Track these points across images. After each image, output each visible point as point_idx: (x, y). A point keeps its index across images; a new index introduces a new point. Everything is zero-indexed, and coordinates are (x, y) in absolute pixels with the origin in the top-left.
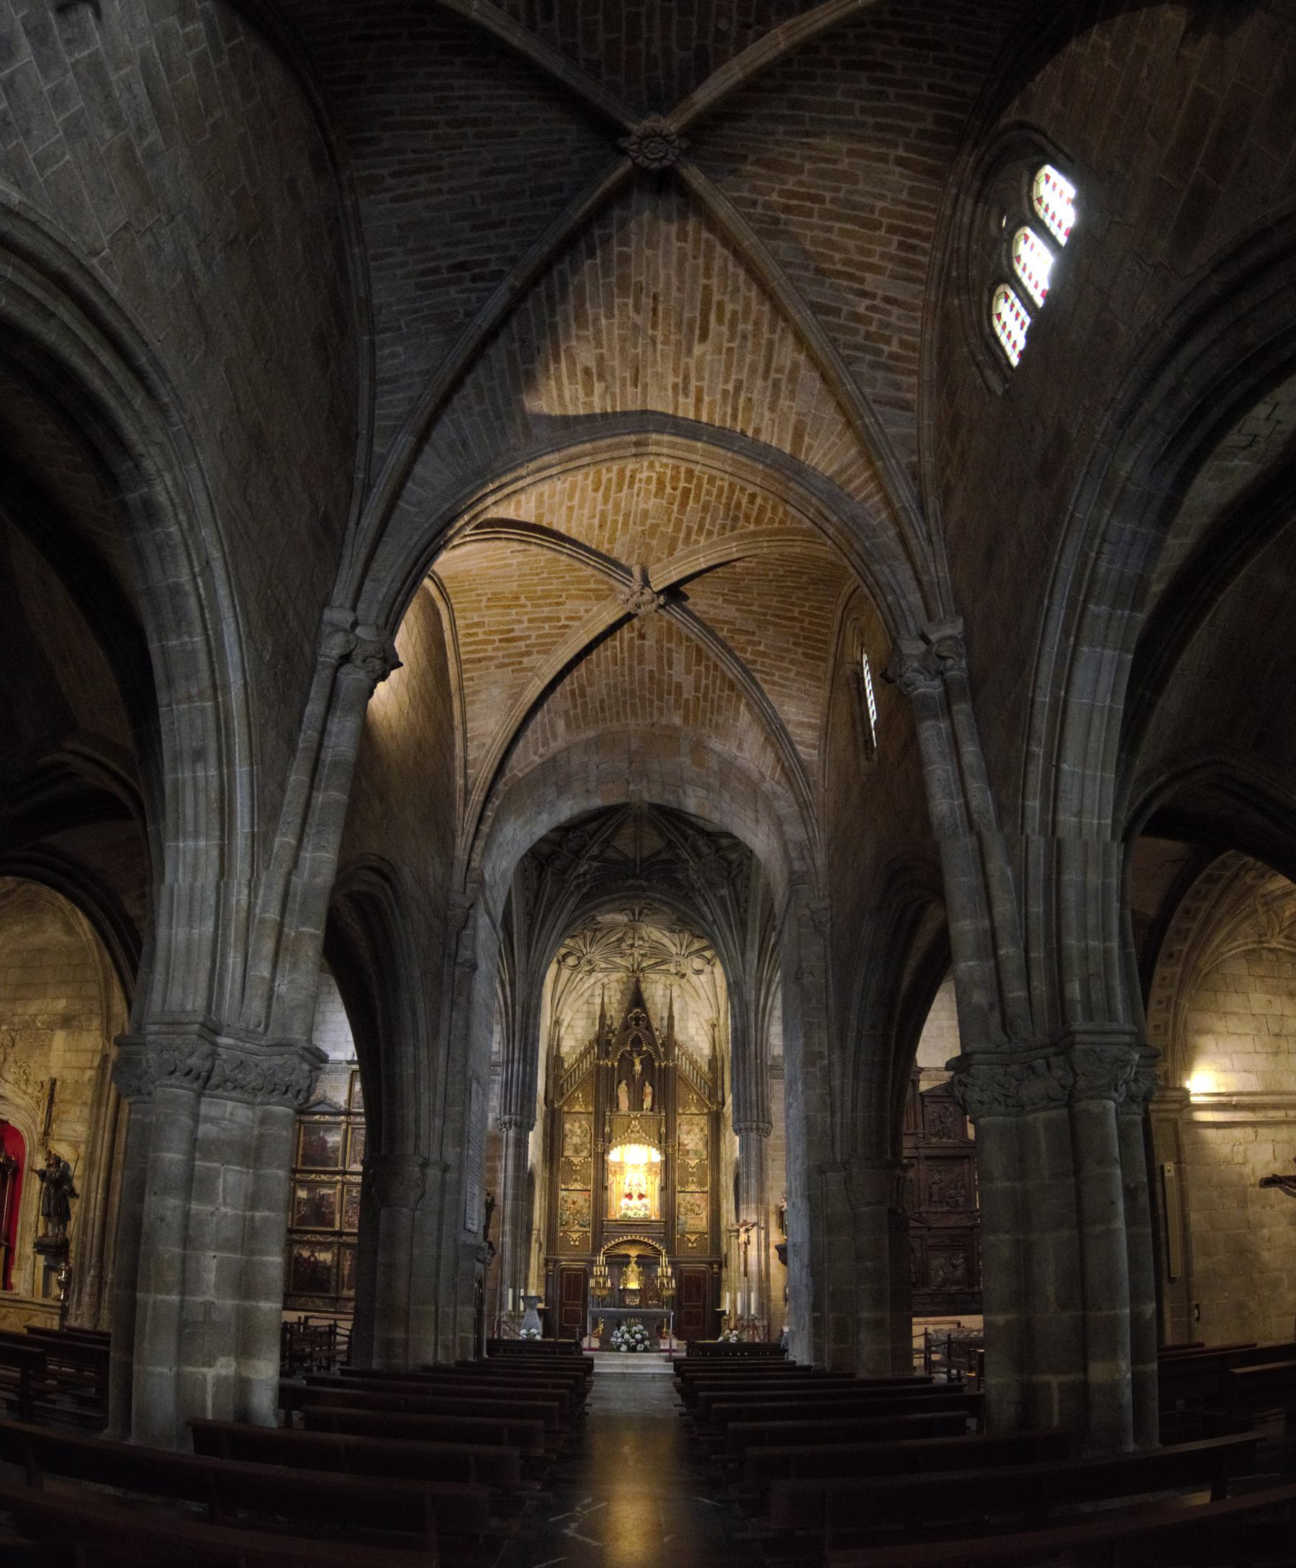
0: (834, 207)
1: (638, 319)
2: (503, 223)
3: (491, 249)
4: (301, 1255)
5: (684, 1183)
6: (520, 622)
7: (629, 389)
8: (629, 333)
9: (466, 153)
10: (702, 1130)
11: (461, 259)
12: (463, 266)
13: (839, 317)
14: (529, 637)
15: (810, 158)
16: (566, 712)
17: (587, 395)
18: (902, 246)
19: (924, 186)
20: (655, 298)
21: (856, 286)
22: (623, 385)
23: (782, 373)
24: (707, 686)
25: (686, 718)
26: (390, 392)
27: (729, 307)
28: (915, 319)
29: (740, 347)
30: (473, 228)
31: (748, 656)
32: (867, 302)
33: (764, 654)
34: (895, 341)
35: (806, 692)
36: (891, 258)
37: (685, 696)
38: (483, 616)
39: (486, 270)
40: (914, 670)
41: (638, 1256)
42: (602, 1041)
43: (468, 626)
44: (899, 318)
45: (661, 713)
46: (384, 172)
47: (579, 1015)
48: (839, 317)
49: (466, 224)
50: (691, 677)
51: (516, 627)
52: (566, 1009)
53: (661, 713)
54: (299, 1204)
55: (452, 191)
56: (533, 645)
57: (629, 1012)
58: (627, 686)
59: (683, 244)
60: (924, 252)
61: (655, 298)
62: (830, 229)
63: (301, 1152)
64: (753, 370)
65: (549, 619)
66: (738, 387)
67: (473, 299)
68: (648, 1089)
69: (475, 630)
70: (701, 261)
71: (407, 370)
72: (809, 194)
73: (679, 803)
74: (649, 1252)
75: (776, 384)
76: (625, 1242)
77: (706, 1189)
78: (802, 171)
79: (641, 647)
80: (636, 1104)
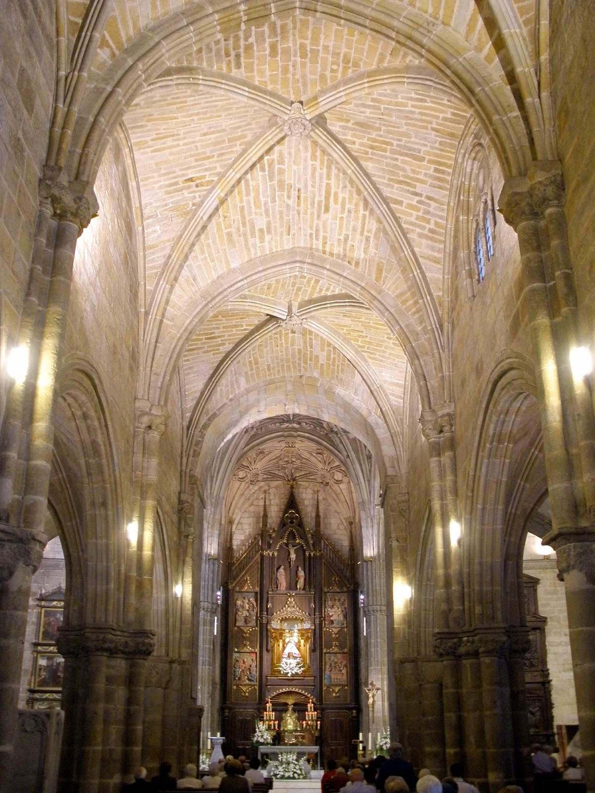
0: (398, 149)
1: (290, 202)
3: (206, 170)
6: (218, 328)
7: (285, 237)
8: (284, 210)
10: (342, 604)
11: (189, 177)
12: (191, 180)
13: (402, 206)
15: (384, 125)
16: (246, 373)
17: (261, 242)
18: (436, 170)
19: (449, 141)
20: (299, 190)
21: (411, 189)
22: (282, 235)
23: (371, 233)
24: (334, 358)
27: (341, 196)
28: (443, 210)
29: (347, 217)
30: (196, 160)
32: (418, 198)
33: (370, 343)
34: (432, 221)
35: (396, 365)
36: (431, 176)
37: (321, 362)
39: (203, 180)
41: (295, 704)
44: (434, 209)
45: (306, 370)
47: (246, 515)
48: (402, 206)
50: (325, 353)
52: (237, 511)
53: (306, 370)
54: (40, 669)
57: (286, 512)
58: (285, 357)
59: (314, 162)
60: (449, 174)
61: (299, 190)
62: (396, 159)
63: (42, 630)
64: (354, 230)
65: (236, 326)
66: (346, 239)
67: (197, 197)
68: (301, 573)
70: (325, 170)
72: (385, 141)
74: (301, 699)
75: (368, 239)
77: (346, 650)
78: (380, 130)
79: (293, 338)
80: (292, 586)
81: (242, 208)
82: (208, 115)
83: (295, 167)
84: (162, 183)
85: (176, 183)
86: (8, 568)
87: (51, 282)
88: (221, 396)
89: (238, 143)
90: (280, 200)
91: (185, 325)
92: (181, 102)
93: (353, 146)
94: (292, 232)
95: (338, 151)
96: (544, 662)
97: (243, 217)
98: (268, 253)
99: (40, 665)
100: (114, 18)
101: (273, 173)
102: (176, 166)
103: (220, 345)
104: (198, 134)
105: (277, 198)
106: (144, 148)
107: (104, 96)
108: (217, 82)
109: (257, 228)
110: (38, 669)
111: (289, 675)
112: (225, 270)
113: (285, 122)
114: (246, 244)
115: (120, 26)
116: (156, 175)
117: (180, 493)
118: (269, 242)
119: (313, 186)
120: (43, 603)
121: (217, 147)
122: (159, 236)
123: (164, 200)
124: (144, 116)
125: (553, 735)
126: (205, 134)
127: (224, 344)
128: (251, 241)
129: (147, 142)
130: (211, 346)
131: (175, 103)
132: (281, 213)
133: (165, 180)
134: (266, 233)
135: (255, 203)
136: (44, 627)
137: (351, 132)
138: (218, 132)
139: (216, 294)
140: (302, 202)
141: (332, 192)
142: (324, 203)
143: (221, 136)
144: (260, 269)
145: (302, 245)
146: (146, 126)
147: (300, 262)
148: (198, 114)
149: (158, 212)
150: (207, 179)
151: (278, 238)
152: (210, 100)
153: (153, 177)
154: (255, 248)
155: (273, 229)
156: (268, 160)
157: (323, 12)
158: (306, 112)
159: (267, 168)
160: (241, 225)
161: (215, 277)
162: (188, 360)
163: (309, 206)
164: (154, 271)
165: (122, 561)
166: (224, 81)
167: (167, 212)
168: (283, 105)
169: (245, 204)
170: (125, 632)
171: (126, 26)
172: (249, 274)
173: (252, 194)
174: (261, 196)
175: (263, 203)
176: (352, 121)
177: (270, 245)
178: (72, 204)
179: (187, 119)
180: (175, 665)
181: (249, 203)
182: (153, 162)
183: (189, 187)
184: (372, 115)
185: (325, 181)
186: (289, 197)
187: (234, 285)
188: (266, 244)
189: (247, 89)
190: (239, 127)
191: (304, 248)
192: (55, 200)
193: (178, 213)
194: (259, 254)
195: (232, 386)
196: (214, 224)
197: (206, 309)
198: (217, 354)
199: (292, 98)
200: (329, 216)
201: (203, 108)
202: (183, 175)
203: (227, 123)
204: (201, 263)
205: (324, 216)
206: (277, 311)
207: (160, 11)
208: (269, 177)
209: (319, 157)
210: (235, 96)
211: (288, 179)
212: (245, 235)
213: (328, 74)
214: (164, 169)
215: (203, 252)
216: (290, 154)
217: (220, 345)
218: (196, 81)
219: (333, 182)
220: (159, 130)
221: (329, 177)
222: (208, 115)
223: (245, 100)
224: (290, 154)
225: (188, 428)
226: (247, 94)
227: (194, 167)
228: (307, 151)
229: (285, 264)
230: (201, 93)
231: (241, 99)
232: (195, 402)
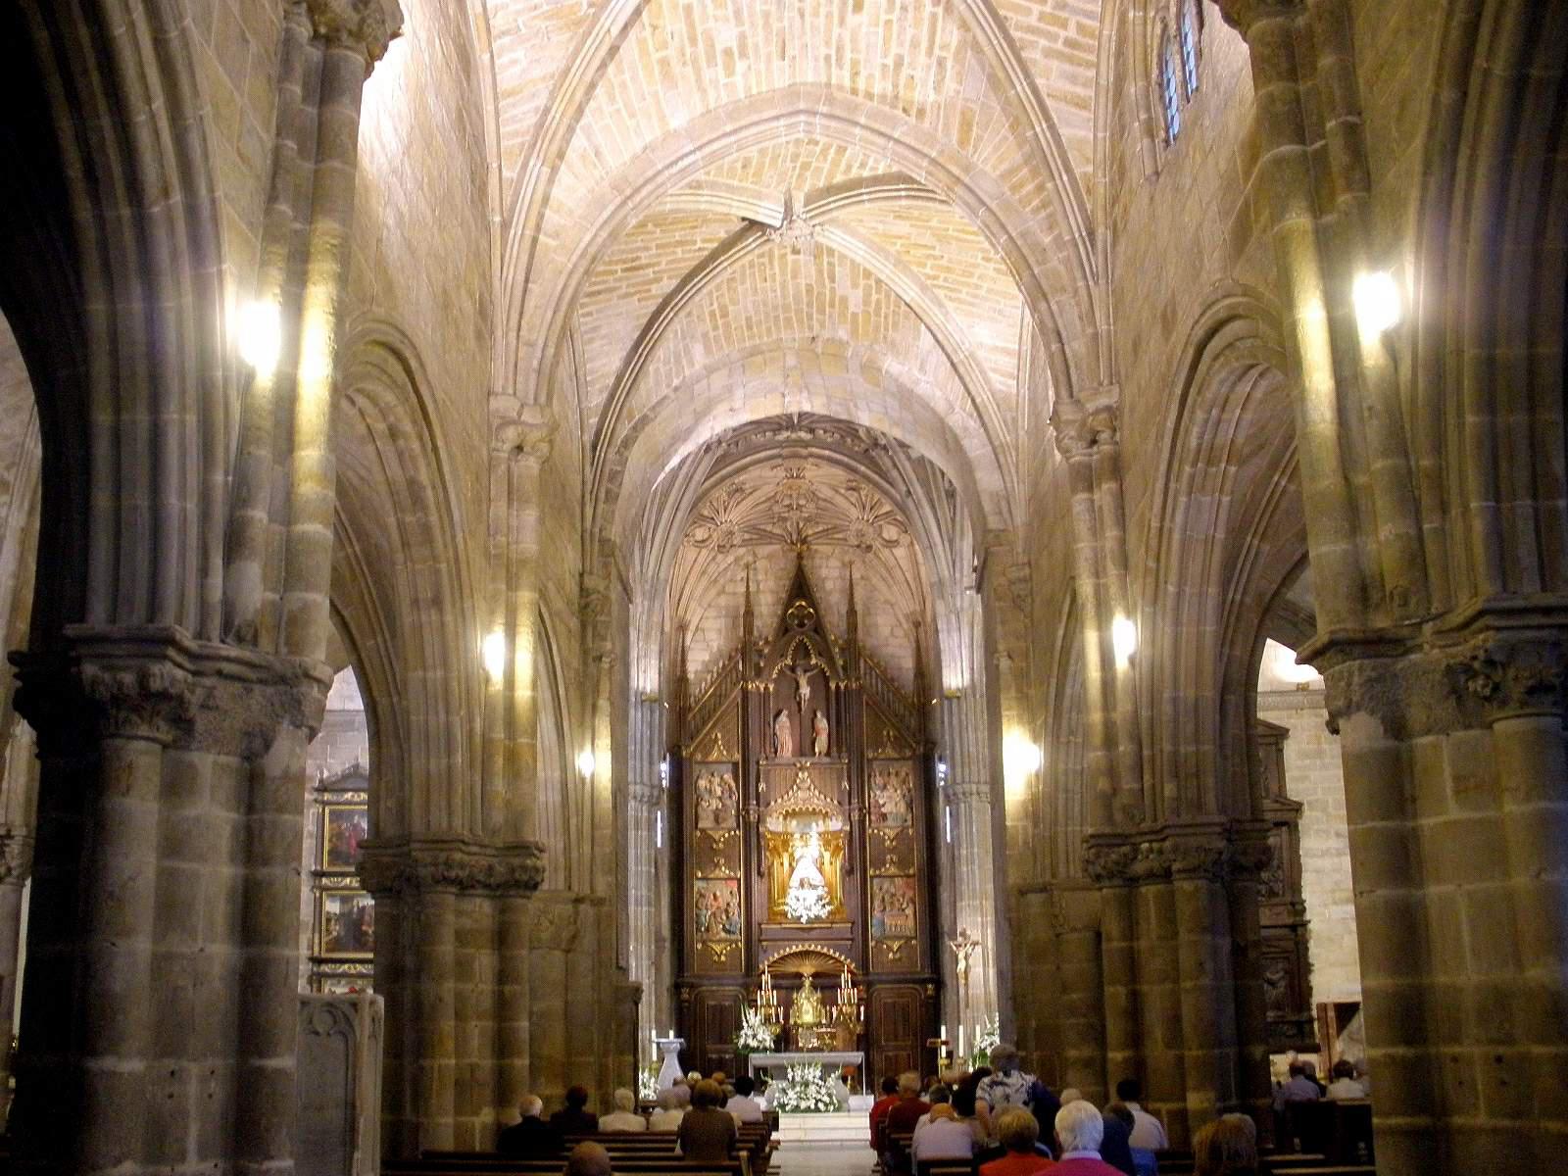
5: (879, 863)
6: (647, 249)
7: (776, 63)
14: (658, 264)
16: (705, 335)
22: (769, 60)
24: (878, 302)
25: (854, 332)
26: (514, 105)
31: (928, 270)
33: (949, 270)
34: (1072, 25)
40: (1071, 438)
41: (815, 976)
42: (745, 653)
45: (822, 325)
47: (712, 613)
50: (860, 292)
51: (642, 255)
53: (822, 325)
57: (789, 604)
65: (680, 243)
68: (822, 724)
73: (850, 414)
75: (941, 63)
76: (795, 955)
80: (805, 748)
88: (657, 383)
91: (582, 245)
94: (789, 52)
96: (1296, 887)
97: (691, 25)
111: (803, 920)
114: (699, 79)
120: (327, 796)
125: (1311, 1021)
127: (657, 280)
128: (707, 74)
130: (633, 285)
136: (330, 841)
139: (641, 181)
144: (728, 128)
145: (810, 79)
151: (763, 66)
162: (590, 314)
164: (520, 140)
170: (485, 846)
177: (754, 78)
187: (675, 162)
188: (738, 79)
194: (725, 100)
205: (852, 19)
212: (695, 61)
215: (612, 99)
225: (594, 448)
232: (605, 395)
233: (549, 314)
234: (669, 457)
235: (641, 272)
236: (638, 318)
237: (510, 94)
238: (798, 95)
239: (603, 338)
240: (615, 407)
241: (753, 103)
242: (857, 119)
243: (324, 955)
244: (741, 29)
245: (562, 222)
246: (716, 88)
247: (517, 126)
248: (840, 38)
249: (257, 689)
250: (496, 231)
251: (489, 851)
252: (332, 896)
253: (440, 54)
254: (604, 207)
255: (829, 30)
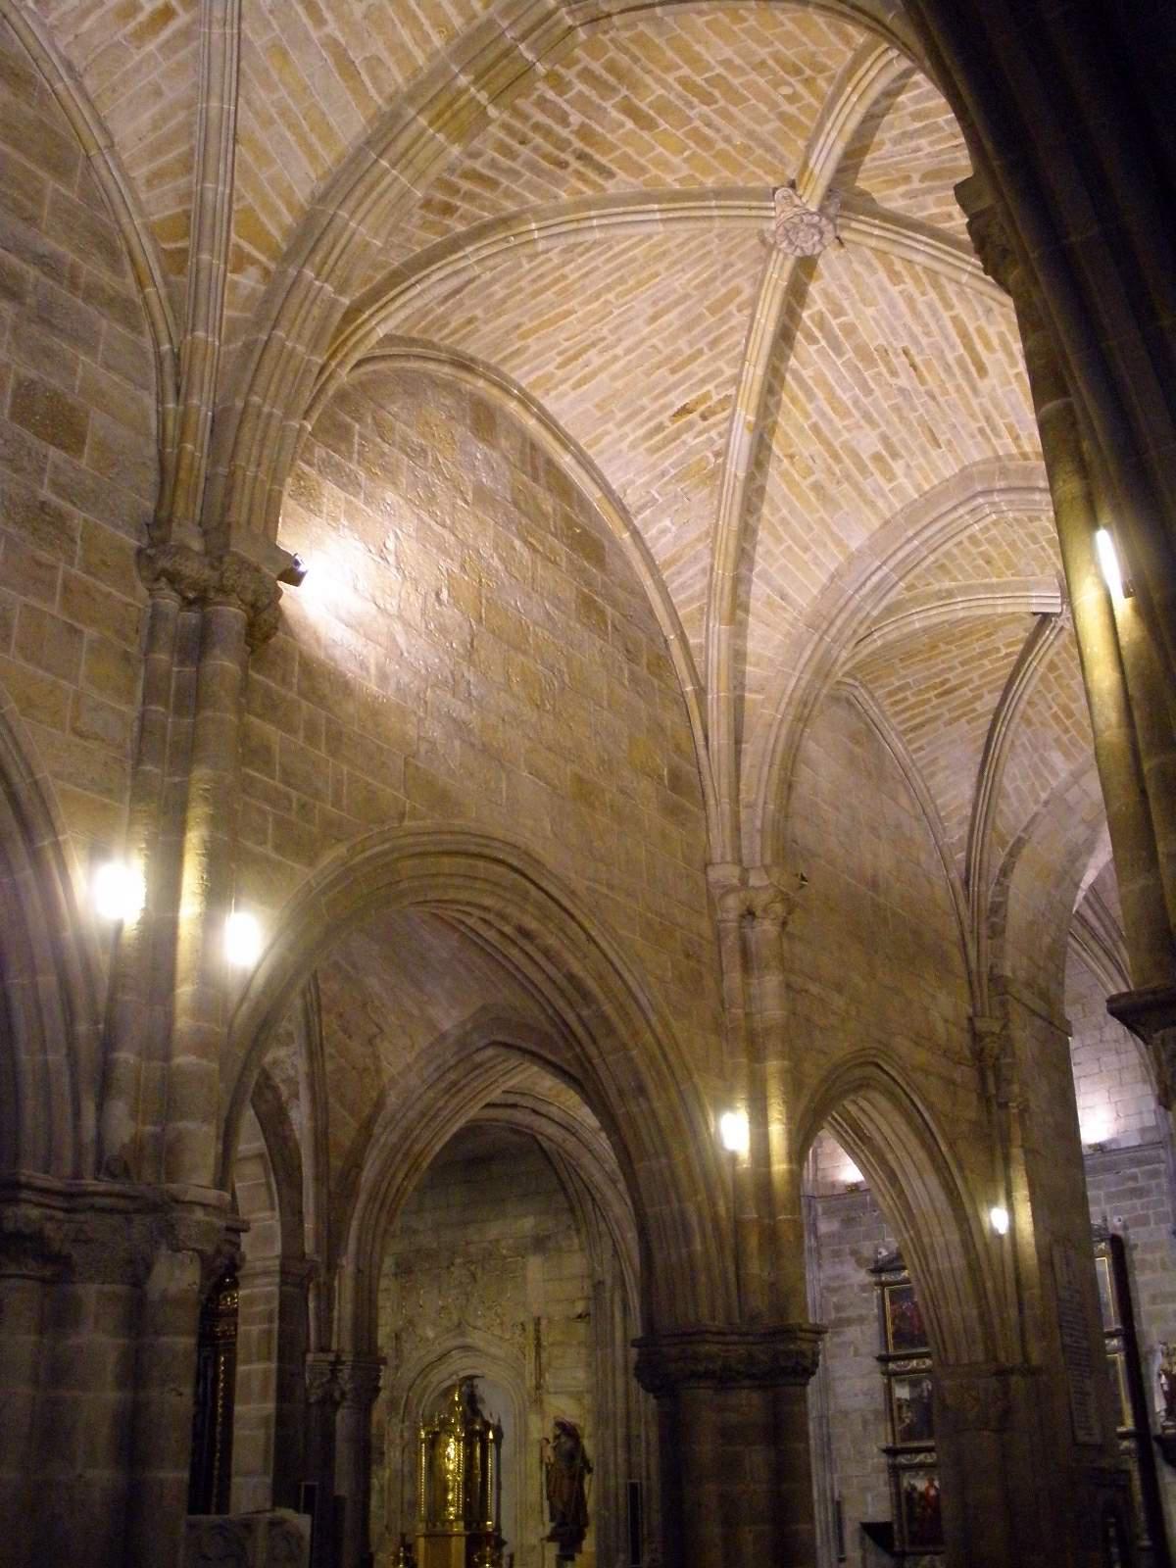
1: (903, 381)
2: (700, 352)
3: (703, 381)
4: (914, 1488)
6: (951, 669)
7: (934, 453)
8: (899, 400)
9: (619, 315)
11: (679, 405)
12: (685, 410)
16: (1057, 740)
20: (906, 352)
22: (925, 452)
30: (673, 371)
38: (905, 677)
43: (890, 694)
46: (551, 368)
49: (663, 370)
51: (950, 676)
54: (900, 1407)
55: (628, 351)
56: (979, 688)
59: (902, 286)
61: (906, 352)
65: (984, 654)
67: (715, 437)
69: (901, 696)
70: (933, 295)
71: (685, 542)
81: (815, 428)
82: (631, 282)
83: (870, 311)
84: (632, 437)
85: (660, 428)
86: (143, 1259)
87: (195, 726)
88: (1022, 801)
89: (732, 307)
90: (880, 385)
91: (789, 692)
92: (556, 281)
93: (953, 223)
94: (942, 439)
95: (922, 247)
97: (828, 445)
98: (916, 496)
99: (899, 1399)
100: (249, 211)
101: (836, 337)
102: (639, 397)
103: (971, 702)
104: (639, 322)
105: (872, 385)
106: (556, 387)
107: (260, 347)
108: (578, 221)
109: (864, 457)
110: (895, 1407)
112: (841, 558)
113: (774, 233)
114: (861, 493)
115: (263, 218)
116: (610, 426)
117: (970, 1019)
118: (907, 475)
119: (928, 334)
120: (884, 1277)
121: (694, 333)
122: (677, 537)
123: (654, 466)
124: (507, 333)
126: (654, 318)
127: (980, 697)
128: (867, 485)
129: (551, 376)
130: (955, 709)
131: (546, 288)
132: (897, 409)
133: (634, 430)
134: (889, 460)
135: (833, 408)
136: (893, 1323)
137: (930, 199)
138: (677, 303)
139: (835, 611)
140: (925, 373)
141: (971, 329)
142: (968, 360)
143: (689, 310)
144: (910, 533)
145: (978, 457)
146: (526, 348)
147: (983, 493)
148: (609, 288)
149: (653, 492)
150: (715, 398)
151: (922, 460)
152: (610, 253)
153: (607, 433)
154: (883, 496)
155: (899, 446)
156: (811, 317)
157: (622, 12)
158: (804, 200)
159: (818, 334)
160: (830, 461)
161: (824, 579)
162: (921, 748)
163: (943, 376)
164: (696, 605)
165: (719, 1194)
166: (593, 213)
167: (671, 487)
168: (754, 204)
169: (815, 418)
170: (747, 1334)
171: (274, 213)
172: (890, 552)
173: (820, 394)
174: (839, 391)
175: (849, 404)
176: (916, 177)
177: (912, 478)
178: (207, 573)
179: (595, 305)
180: (1014, 1379)
181: (823, 414)
182: (589, 405)
183: (690, 425)
184: (938, 148)
185: (946, 315)
186: (894, 373)
187: (864, 584)
188: (902, 480)
189: (656, 207)
190: (713, 279)
191: (984, 462)
192: (173, 579)
193: (695, 480)
194: (898, 506)
195: (1038, 774)
196: (778, 479)
197: (823, 646)
198: (973, 719)
199: (771, 181)
200: (992, 381)
201: (609, 274)
202: (664, 408)
203: (683, 281)
204: (783, 561)
205: (983, 385)
206: (1034, 601)
207: (328, 158)
208: (833, 349)
209: (904, 273)
210: (630, 230)
211: (874, 337)
212: (848, 477)
213: (786, 107)
214: (620, 410)
215: (779, 540)
216: (843, 289)
217: (971, 702)
218: (525, 238)
219: (960, 309)
220: (558, 344)
221: (949, 306)
222: (631, 282)
223: (660, 227)
224: (843, 289)
225: (966, 883)
226: (658, 216)
227: (675, 386)
228: (874, 272)
229: (955, 508)
230: (581, 249)
231: (651, 230)
232: (966, 828)
233: (766, 769)
234: (1081, 873)
235: (956, 693)
236: (975, 740)
237: (669, 563)
238: (971, 478)
239: (946, 768)
240: (978, 835)
241: (929, 499)
242: (1033, 484)
243: (899, 1446)
244: (878, 431)
245: (765, 673)
246: (883, 496)
247: (690, 592)
248: (984, 410)
249: (137, 1218)
250: (692, 703)
251: (750, 1338)
252: (901, 1381)
253: (526, 553)
254: (803, 649)
255: (968, 405)
